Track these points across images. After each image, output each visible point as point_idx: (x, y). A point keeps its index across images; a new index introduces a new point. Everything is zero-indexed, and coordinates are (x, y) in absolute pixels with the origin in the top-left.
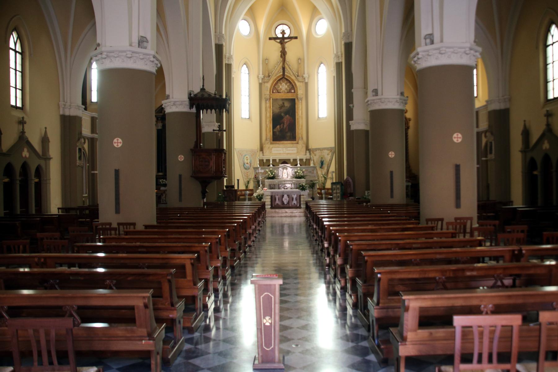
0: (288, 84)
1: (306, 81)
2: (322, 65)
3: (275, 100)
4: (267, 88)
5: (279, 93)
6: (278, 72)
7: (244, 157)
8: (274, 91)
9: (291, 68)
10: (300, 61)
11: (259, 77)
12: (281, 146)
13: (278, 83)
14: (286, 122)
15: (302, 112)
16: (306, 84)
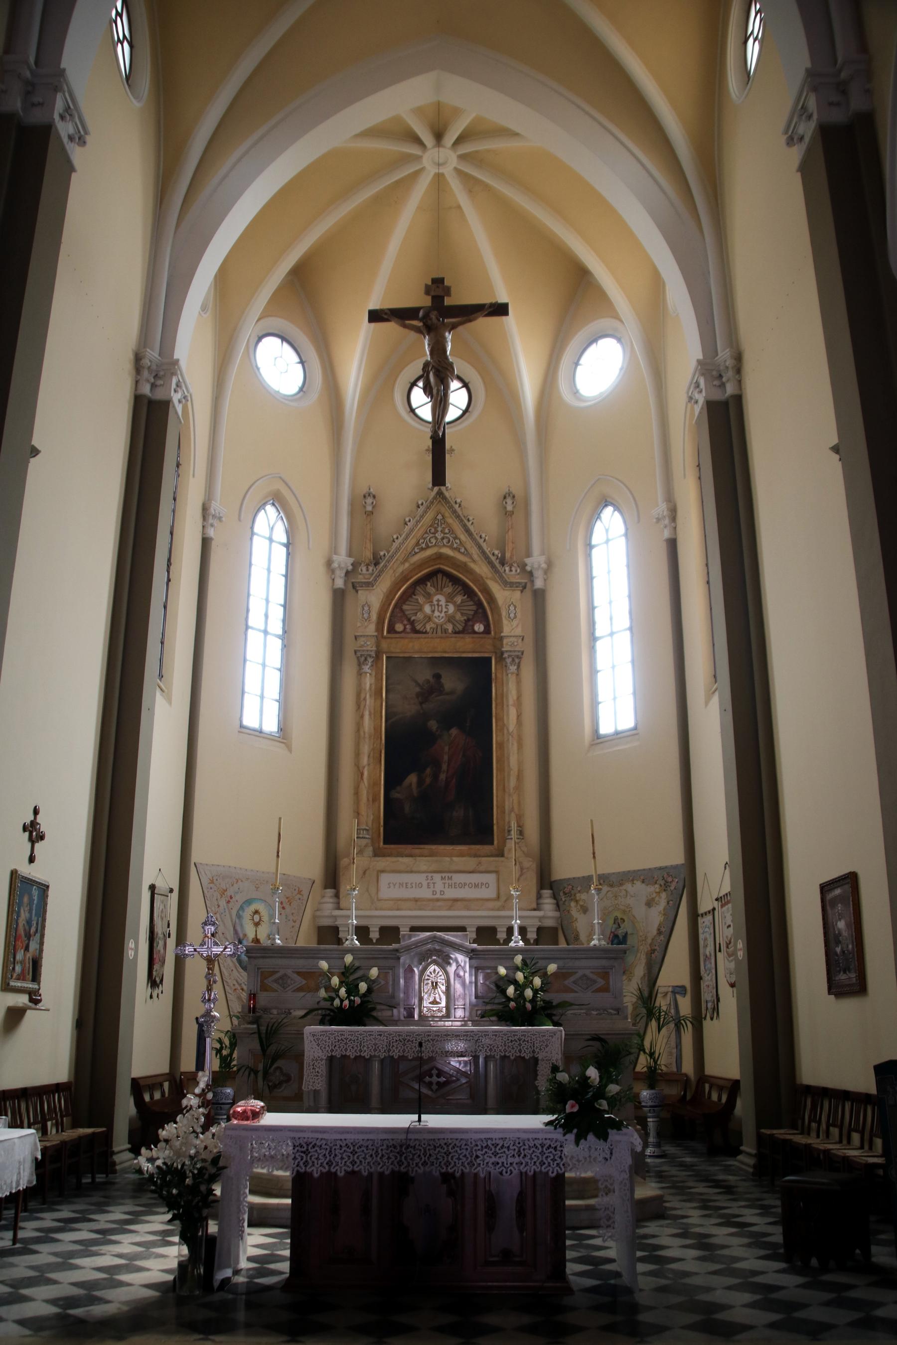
0: (459, 599)
1: (539, 584)
2: (608, 512)
3: (398, 664)
4: (366, 608)
5: (415, 631)
6: (417, 544)
7: (242, 908)
8: (399, 627)
9: (472, 528)
10: (509, 501)
11: (335, 565)
12: (423, 863)
13: (414, 594)
14: (446, 758)
15: (519, 716)
16: (539, 599)
